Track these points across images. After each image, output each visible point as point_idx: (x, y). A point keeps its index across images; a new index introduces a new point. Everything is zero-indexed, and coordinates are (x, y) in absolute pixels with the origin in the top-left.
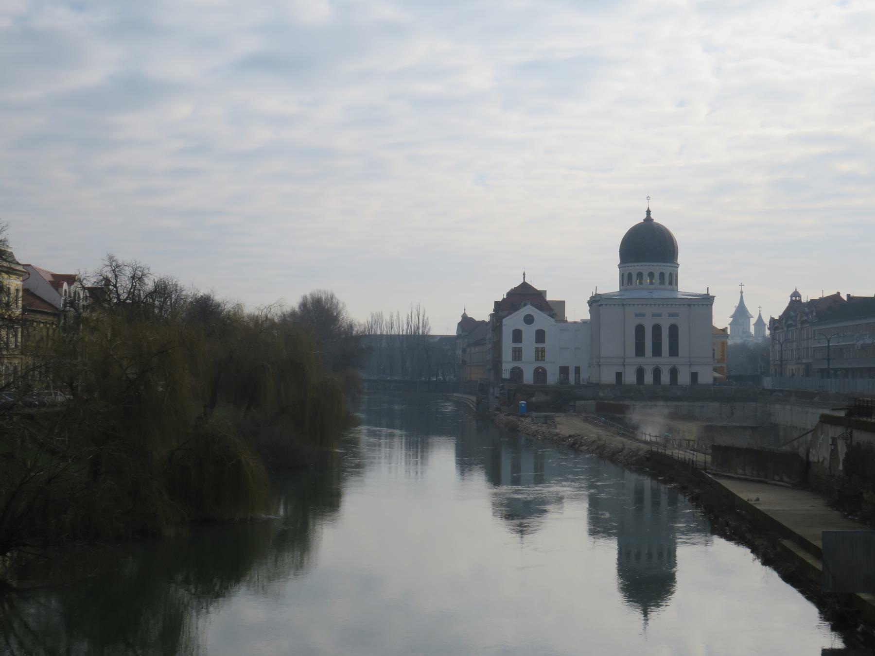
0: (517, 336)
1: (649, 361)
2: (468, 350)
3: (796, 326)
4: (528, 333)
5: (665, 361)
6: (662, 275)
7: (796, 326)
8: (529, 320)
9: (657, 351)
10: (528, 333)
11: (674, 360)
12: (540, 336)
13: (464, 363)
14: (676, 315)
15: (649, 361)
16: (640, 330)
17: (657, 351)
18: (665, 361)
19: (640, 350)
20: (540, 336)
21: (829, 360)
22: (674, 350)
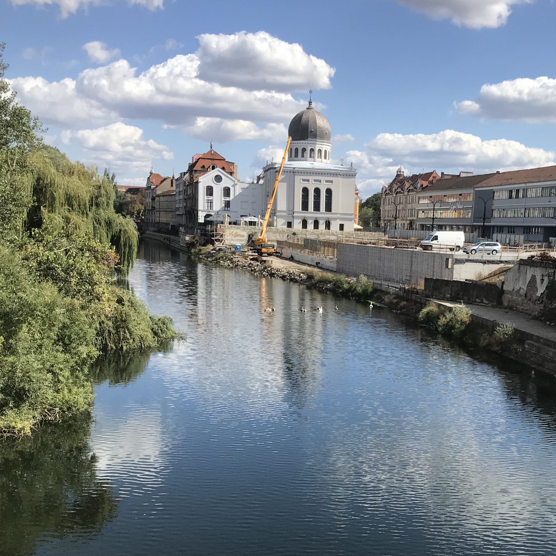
0: (210, 191)
1: (311, 214)
2: (157, 199)
3: (392, 194)
4: (218, 190)
5: (322, 215)
6: (320, 151)
7: (392, 194)
8: (218, 179)
9: (317, 208)
10: (218, 190)
11: (328, 215)
12: (227, 192)
13: (153, 208)
14: (332, 182)
15: (311, 214)
16: (305, 191)
17: (317, 208)
18: (322, 215)
19: (305, 207)
20: (227, 192)
21: (484, 219)
22: (329, 208)
